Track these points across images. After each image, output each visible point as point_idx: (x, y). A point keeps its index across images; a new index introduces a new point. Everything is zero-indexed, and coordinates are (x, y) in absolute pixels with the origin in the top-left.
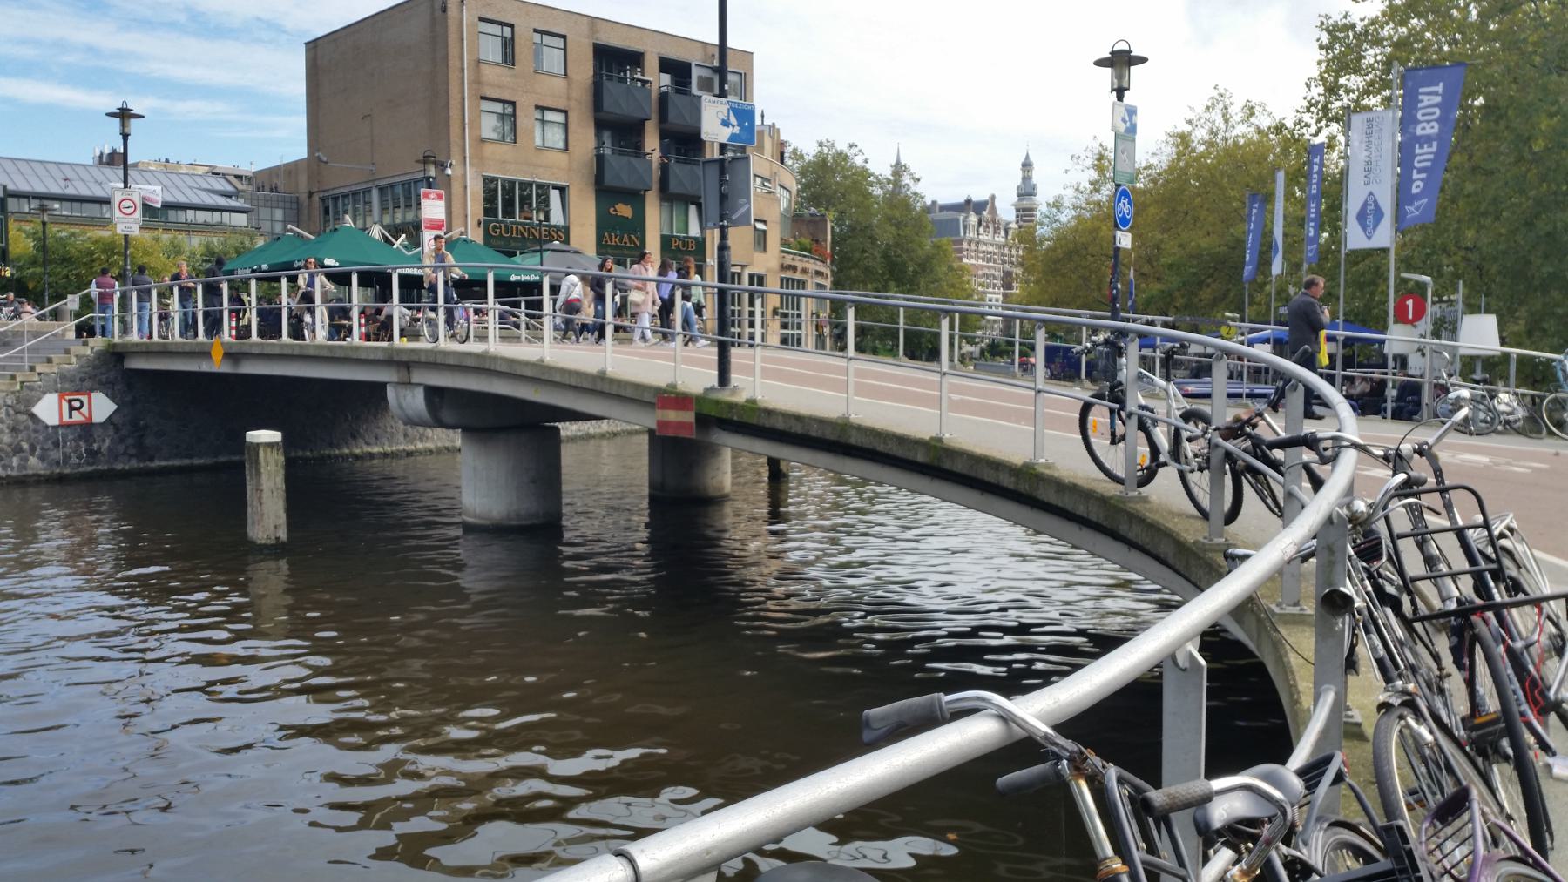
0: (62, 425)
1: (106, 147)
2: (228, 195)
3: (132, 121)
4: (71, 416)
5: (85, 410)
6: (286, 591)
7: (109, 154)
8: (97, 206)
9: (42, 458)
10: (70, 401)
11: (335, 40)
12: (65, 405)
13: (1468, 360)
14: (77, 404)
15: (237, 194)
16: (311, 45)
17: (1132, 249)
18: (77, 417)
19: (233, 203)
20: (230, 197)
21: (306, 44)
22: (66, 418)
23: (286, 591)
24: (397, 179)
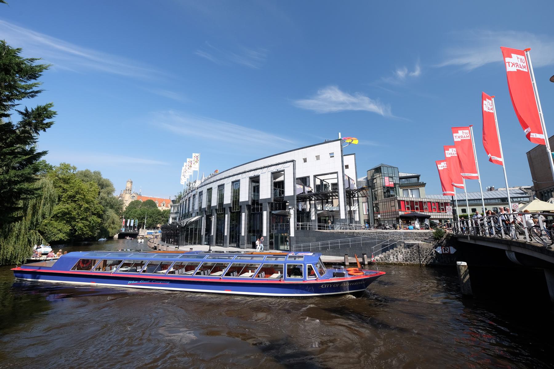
0: (443, 253)
1: (489, 187)
2: (523, 194)
3: (209, 246)
4: (445, 252)
5: (448, 250)
6: (35, 109)
7: (490, 188)
8: (473, 201)
9: (439, 261)
10: (444, 248)
11: (535, 150)
12: (443, 249)
13: (271, 237)
14: (446, 249)
15: (525, 193)
16: (528, 153)
17: (294, 236)
18: (446, 252)
19: (524, 195)
20: (523, 194)
21: (526, 153)
22: (444, 252)
23: (35, 109)
24: (93, 259)
